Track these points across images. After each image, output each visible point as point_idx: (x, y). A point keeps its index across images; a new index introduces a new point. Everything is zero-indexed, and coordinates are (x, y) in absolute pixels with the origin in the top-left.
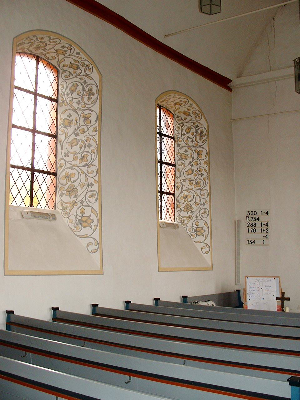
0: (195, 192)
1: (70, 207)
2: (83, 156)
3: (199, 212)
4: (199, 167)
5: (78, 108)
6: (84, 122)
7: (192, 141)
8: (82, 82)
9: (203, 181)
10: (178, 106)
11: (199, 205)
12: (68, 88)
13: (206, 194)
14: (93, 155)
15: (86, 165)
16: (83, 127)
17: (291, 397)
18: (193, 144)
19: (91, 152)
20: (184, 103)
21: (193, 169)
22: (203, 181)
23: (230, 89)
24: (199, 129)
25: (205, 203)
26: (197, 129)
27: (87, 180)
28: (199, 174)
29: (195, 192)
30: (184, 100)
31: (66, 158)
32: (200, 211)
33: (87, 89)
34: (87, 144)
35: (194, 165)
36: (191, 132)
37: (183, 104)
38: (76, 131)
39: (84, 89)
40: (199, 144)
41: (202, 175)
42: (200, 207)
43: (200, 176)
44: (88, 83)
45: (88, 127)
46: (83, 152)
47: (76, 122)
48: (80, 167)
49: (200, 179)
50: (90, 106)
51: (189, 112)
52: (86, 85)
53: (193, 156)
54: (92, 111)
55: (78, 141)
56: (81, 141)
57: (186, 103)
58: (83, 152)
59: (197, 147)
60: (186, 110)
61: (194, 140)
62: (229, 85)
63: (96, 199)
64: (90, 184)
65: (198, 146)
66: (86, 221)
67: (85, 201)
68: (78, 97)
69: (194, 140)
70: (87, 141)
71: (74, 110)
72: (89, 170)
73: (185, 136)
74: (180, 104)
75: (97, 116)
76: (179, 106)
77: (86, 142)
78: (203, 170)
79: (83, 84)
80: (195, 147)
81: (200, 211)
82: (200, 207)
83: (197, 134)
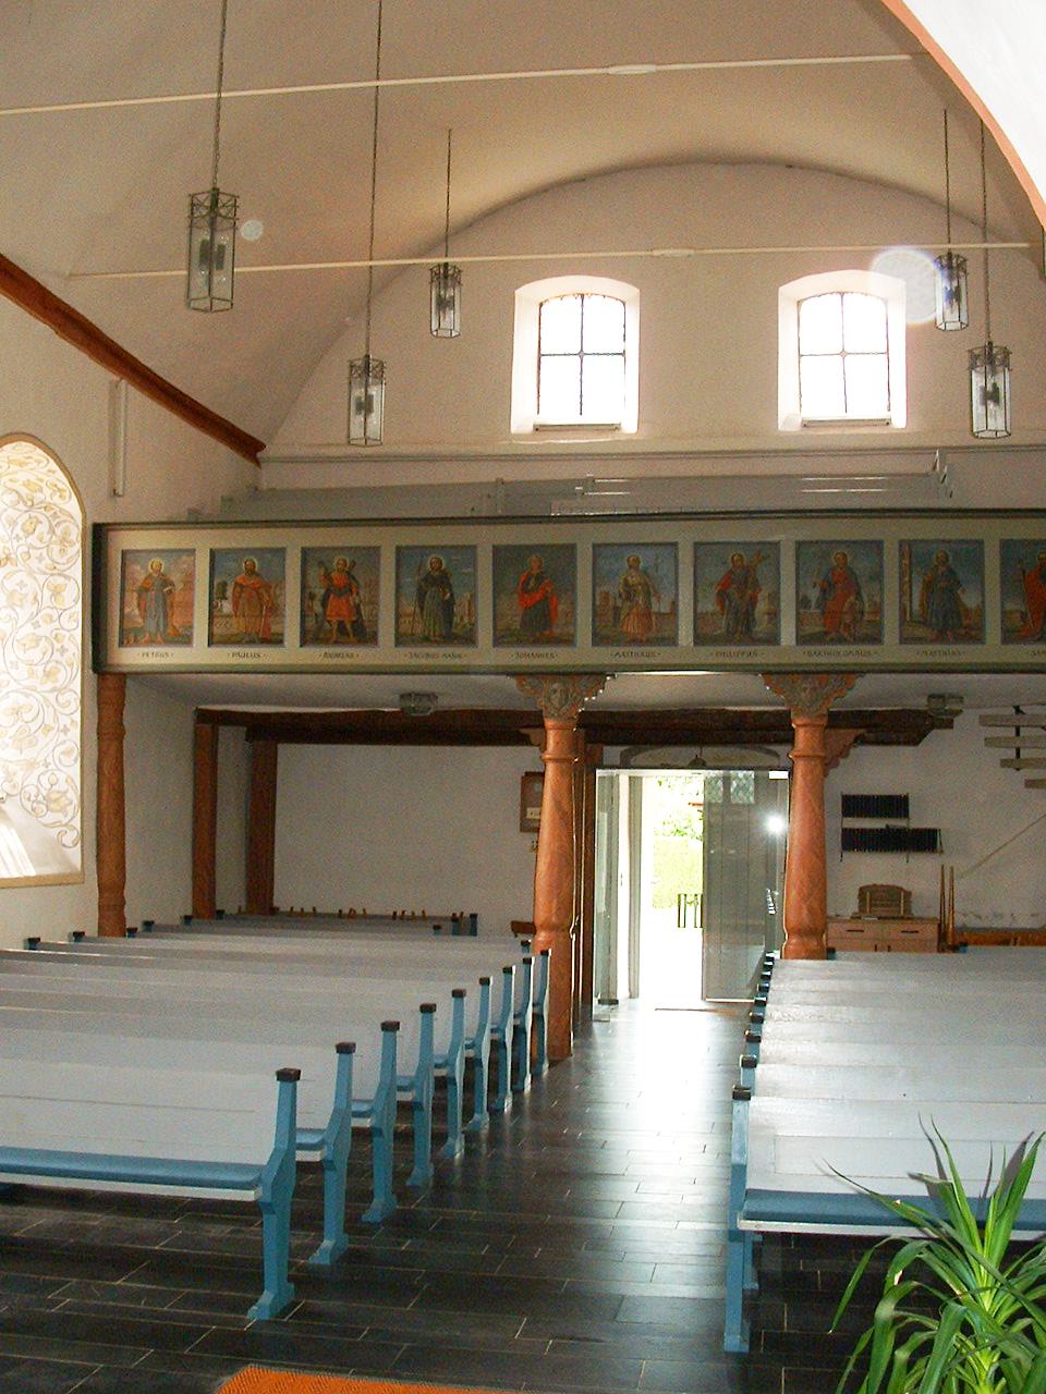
1: (22, 773)
5: (38, 569)
7: (40, 559)
8: (48, 514)
10: (14, 468)
12: (19, 527)
13: (72, 701)
14: (69, 669)
16: (49, 611)
17: (1026, 1201)
20: (36, 464)
21: (38, 634)
23: (257, 462)
25: (68, 726)
26: (54, 523)
27: (56, 719)
30: (36, 457)
31: (13, 672)
33: (58, 531)
34: (57, 646)
37: (30, 466)
39: (52, 531)
40: (58, 566)
47: (35, 598)
50: (63, 567)
53: (39, 598)
55: (38, 640)
57: (41, 465)
59: (52, 575)
60: (33, 479)
62: (259, 455)
64: (62, 727)
66: (56, 801)
71: (31, 573)
73: (21, 542)
74: (21, 464)
76: (18, 468)
77: (55, 642)
78: (66, 639)
80: (45, 573)
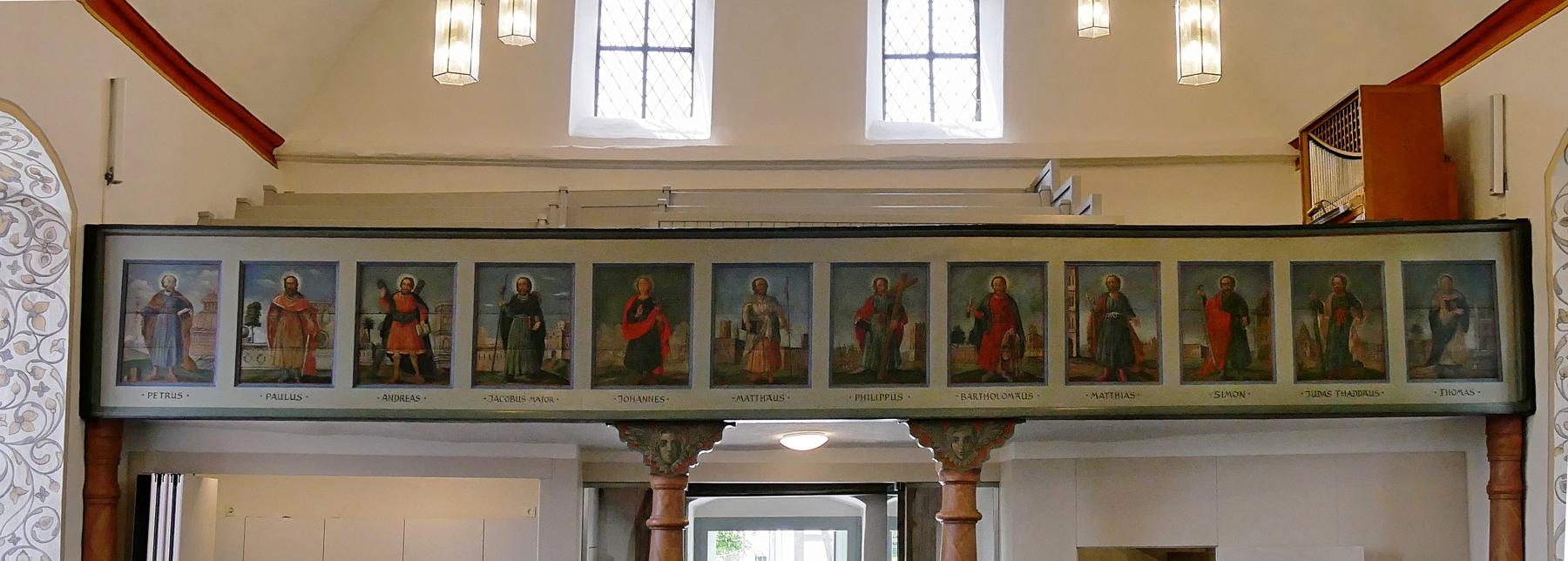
0: (12, 449)
2: (20, 414)
3: (25, 521)
4: (32, 361)
6: (28, 319)
9: (45, 413)
11: (28, 494)
15: (28, 441)
16: (24, 337)
18: (16, 278)
19: (44, 407)
22: (45, 413)
23: (273, 160)
24: (41, 223)
26: (34, 223)
28: (31, 386)
29: (12, 449)
32: (27, 517)
33: (40, 233)
35: (13, 353)
36: (10, 233)
38: (4, 346)
40: (38, 279)
41: (42, 389)
42: (30, 503)
43: (33, 395)
44: (43, 217)
45: (40, 338)
46: (20, 405)
48: (11, 444)
49: (34, 404)
51: (18, 170)
52: (36, 222)
54: (51, 294)
56: (16, 373)
57: (21, 144)
58: (20, 405)
61: (21, 263)
63: (54, 531)
64: (37, 491)
65: (35, 286)
67: (22, 536)
68: (13, 250)
69: (21, 263)
70: (33, 373)
72: (38, 453)
75: (66, 310)
77: (31, 378)
79: (30, 217)
80: (20, 288)
81: (27, 517)
82: (30, 503)
83: (33, 242)
